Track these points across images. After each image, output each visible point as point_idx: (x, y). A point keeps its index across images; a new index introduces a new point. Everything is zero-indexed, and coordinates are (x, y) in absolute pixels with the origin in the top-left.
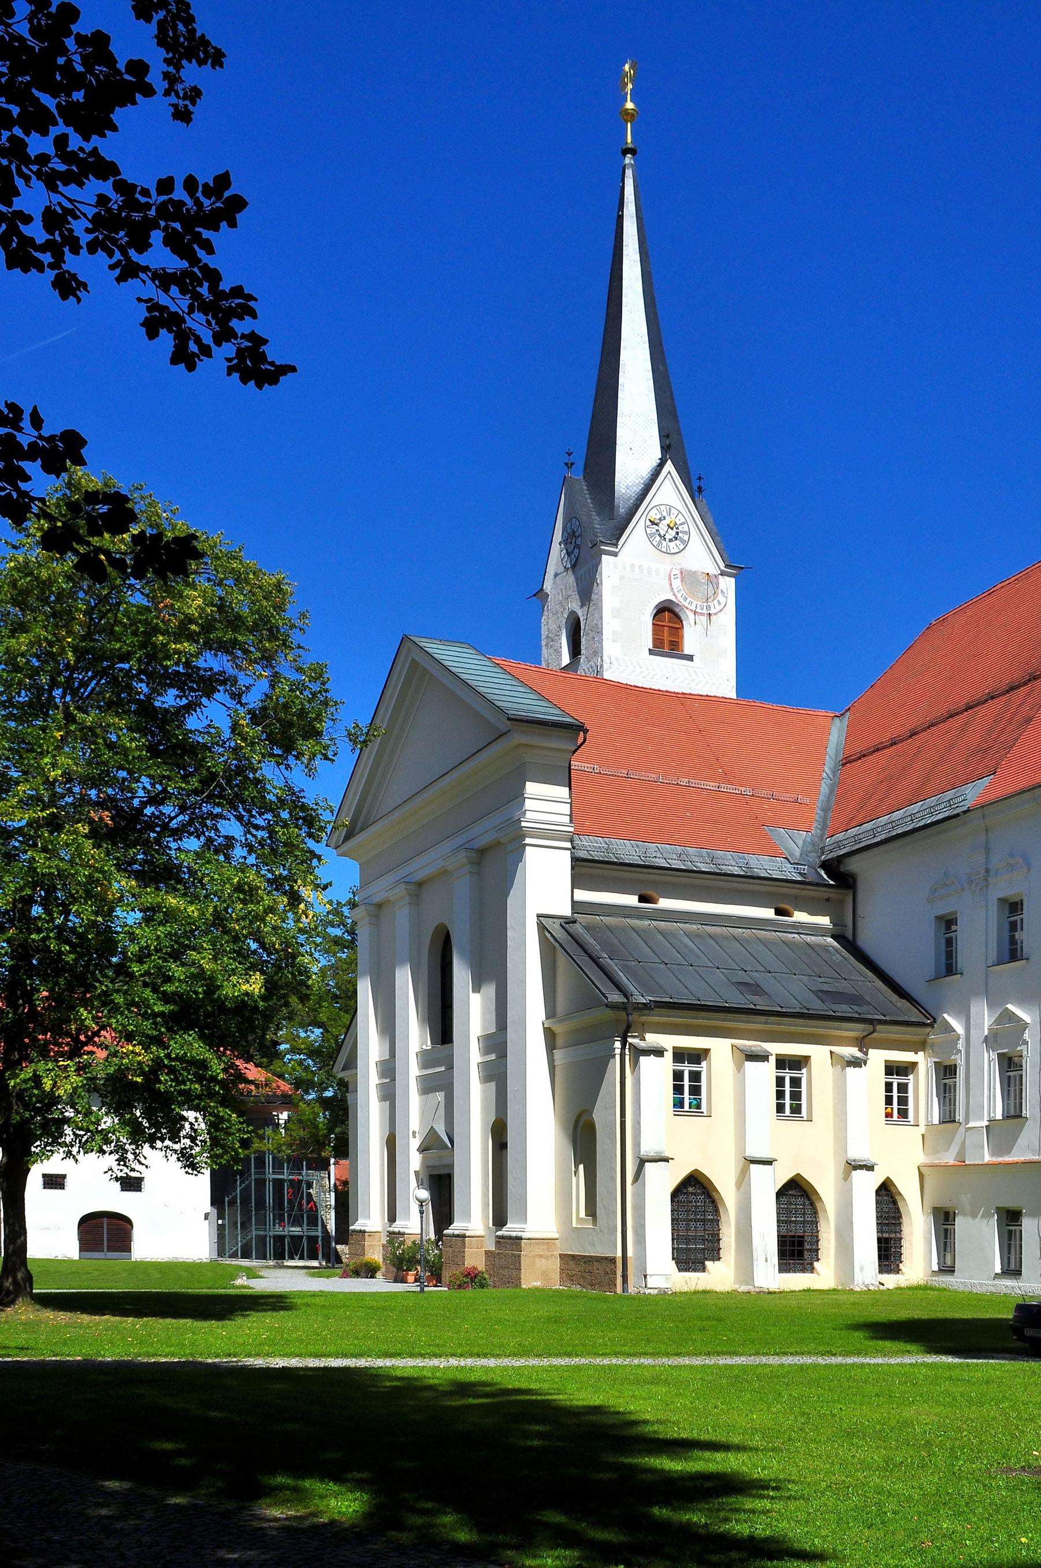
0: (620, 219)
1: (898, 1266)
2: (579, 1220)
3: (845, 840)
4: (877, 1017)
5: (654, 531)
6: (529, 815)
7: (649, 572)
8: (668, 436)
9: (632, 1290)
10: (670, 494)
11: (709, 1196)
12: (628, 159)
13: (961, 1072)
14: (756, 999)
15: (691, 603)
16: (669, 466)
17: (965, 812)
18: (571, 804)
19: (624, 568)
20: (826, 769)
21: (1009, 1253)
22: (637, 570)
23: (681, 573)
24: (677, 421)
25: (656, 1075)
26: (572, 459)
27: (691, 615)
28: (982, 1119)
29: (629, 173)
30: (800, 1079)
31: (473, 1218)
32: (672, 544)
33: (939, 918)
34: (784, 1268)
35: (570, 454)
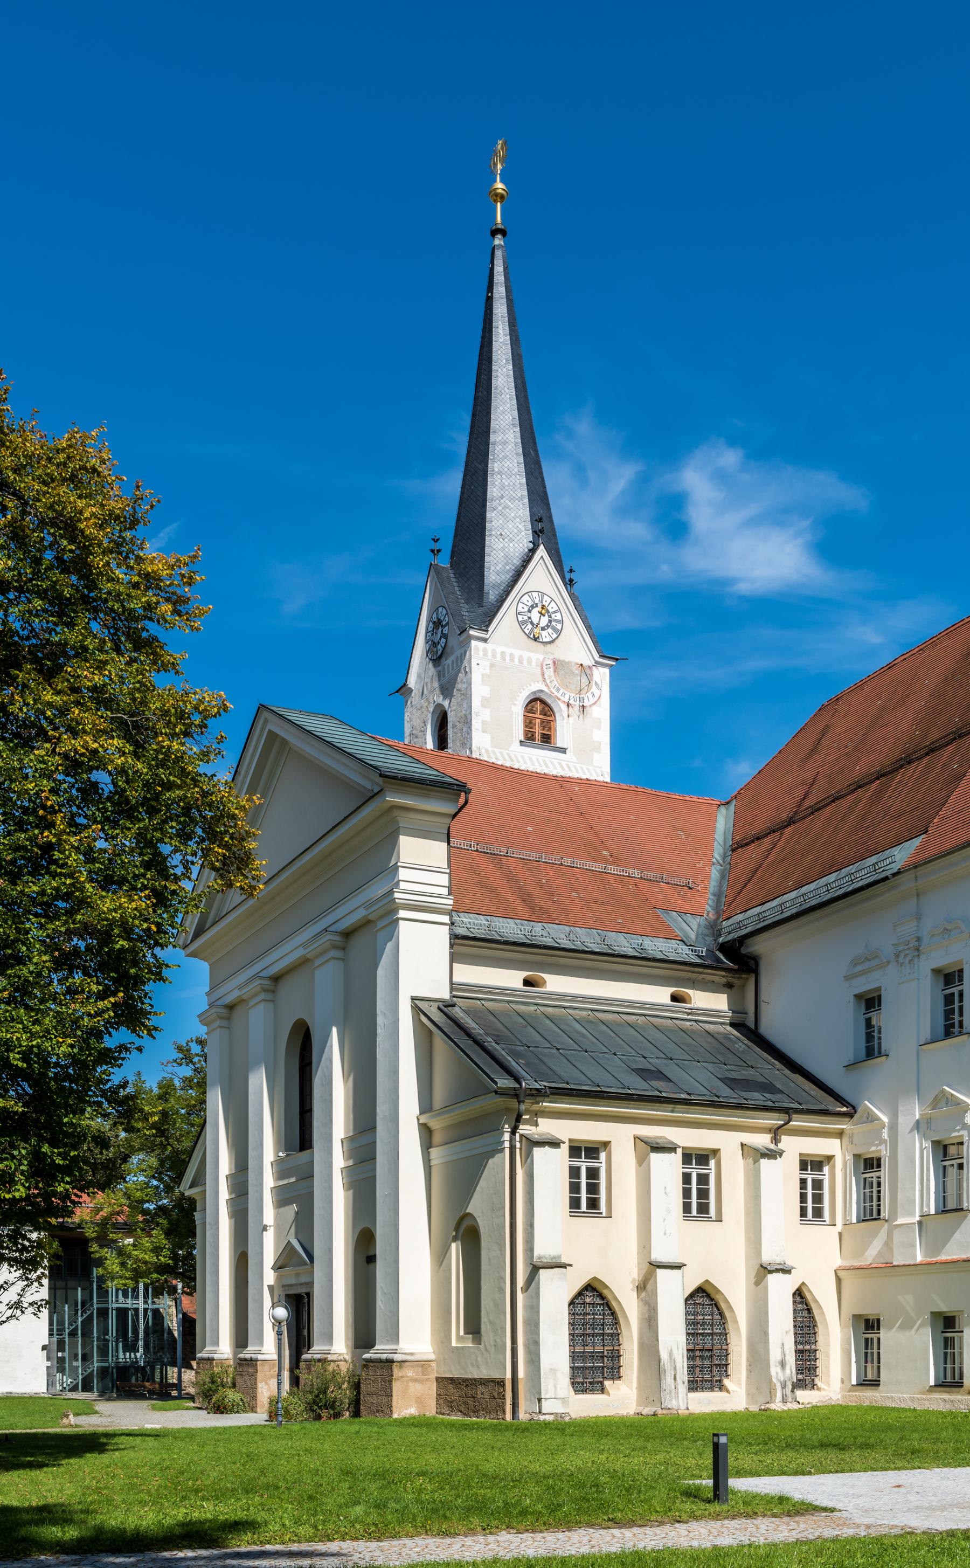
0: (489, 300)
1: (813, 1380)
2: (459, 1338)
3: (746, 919)
4: (792, 1105)
5: (526, 618)
6: (403, 885)
7: (521, 661)
8: (540, 520)
9: (523, 1416)
10: (542, 577)
11: (608, 1305)
12: (498, 241)
13: (886, 1163)
14: (661, 1084)
15: (564, 694)
16: (541, 551)
17: (894, 875)
18: (450, 874)
19: (494, 656)
20: (716, 855)
21: (945, 1363)
22: (508, 659)
23: (554, 662)
24: (549, 508)
25: (551, 1168)
26: (438, 546)
27: (564, 707)
28: (912, 1214)
29: (499, 254)
30: (707, 1176)
31: (336, 1343)
32: (544, 633)
33: (858, 997)
34: (694, 1386)
35: (436, 541)
